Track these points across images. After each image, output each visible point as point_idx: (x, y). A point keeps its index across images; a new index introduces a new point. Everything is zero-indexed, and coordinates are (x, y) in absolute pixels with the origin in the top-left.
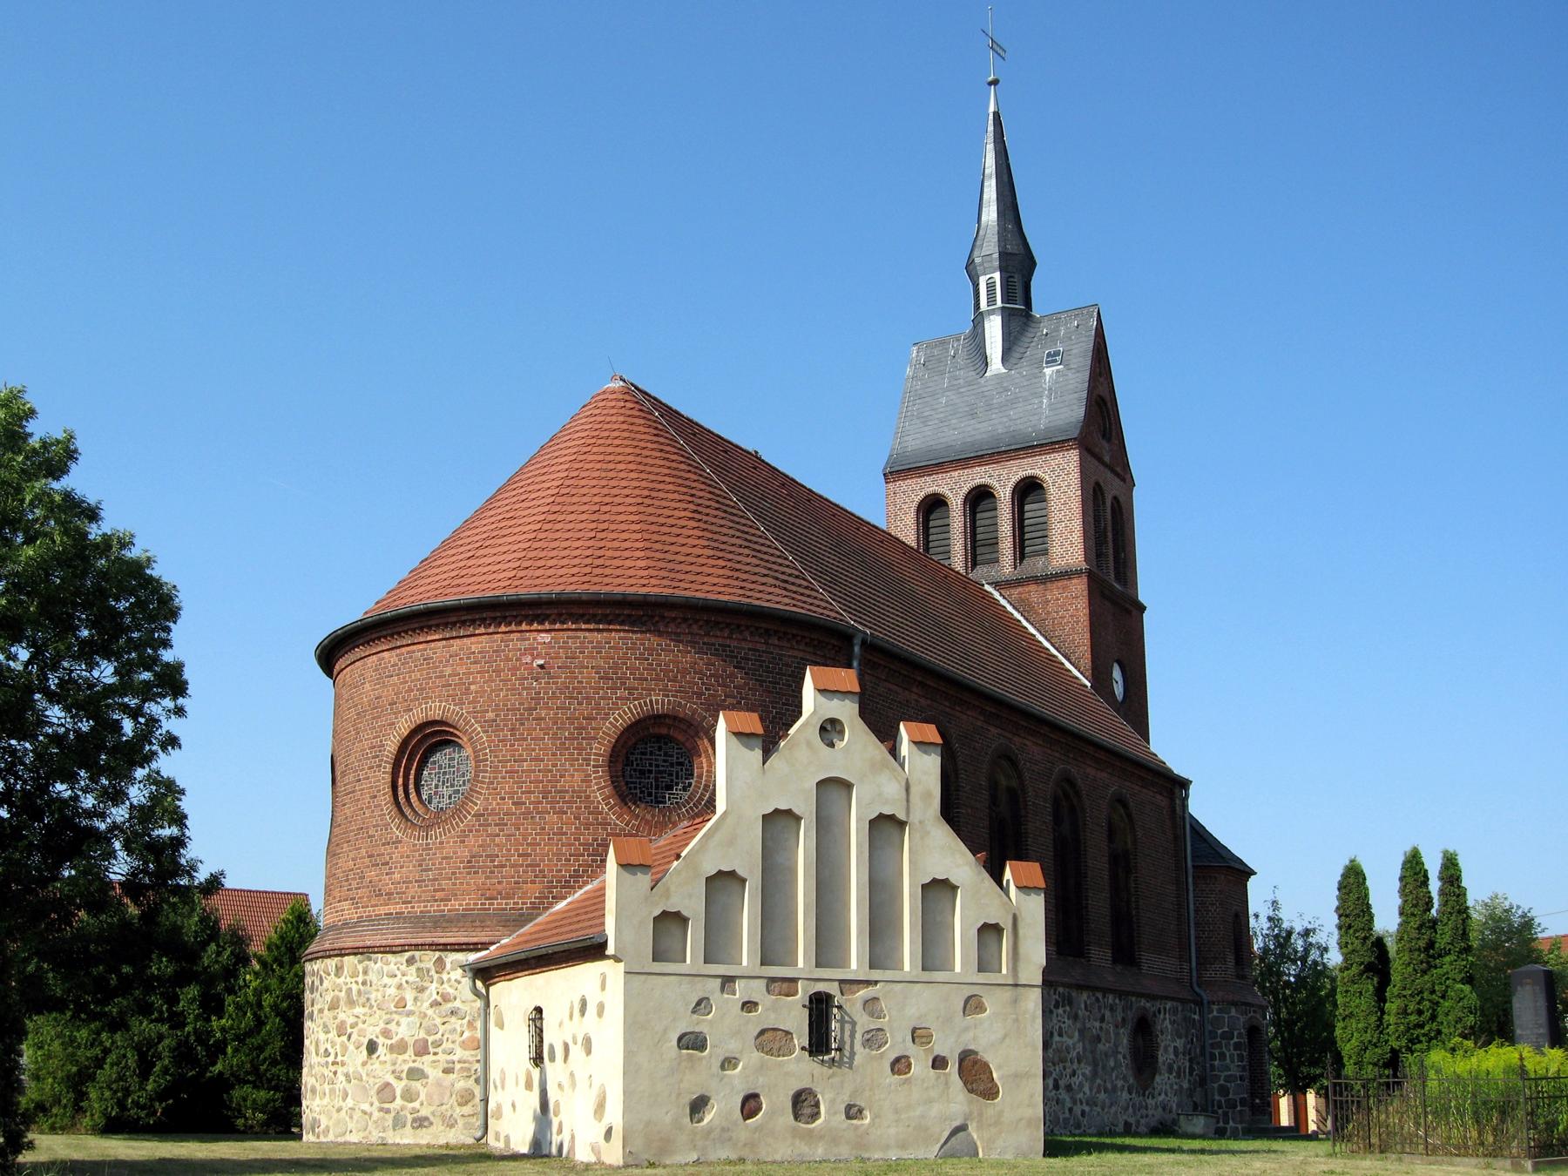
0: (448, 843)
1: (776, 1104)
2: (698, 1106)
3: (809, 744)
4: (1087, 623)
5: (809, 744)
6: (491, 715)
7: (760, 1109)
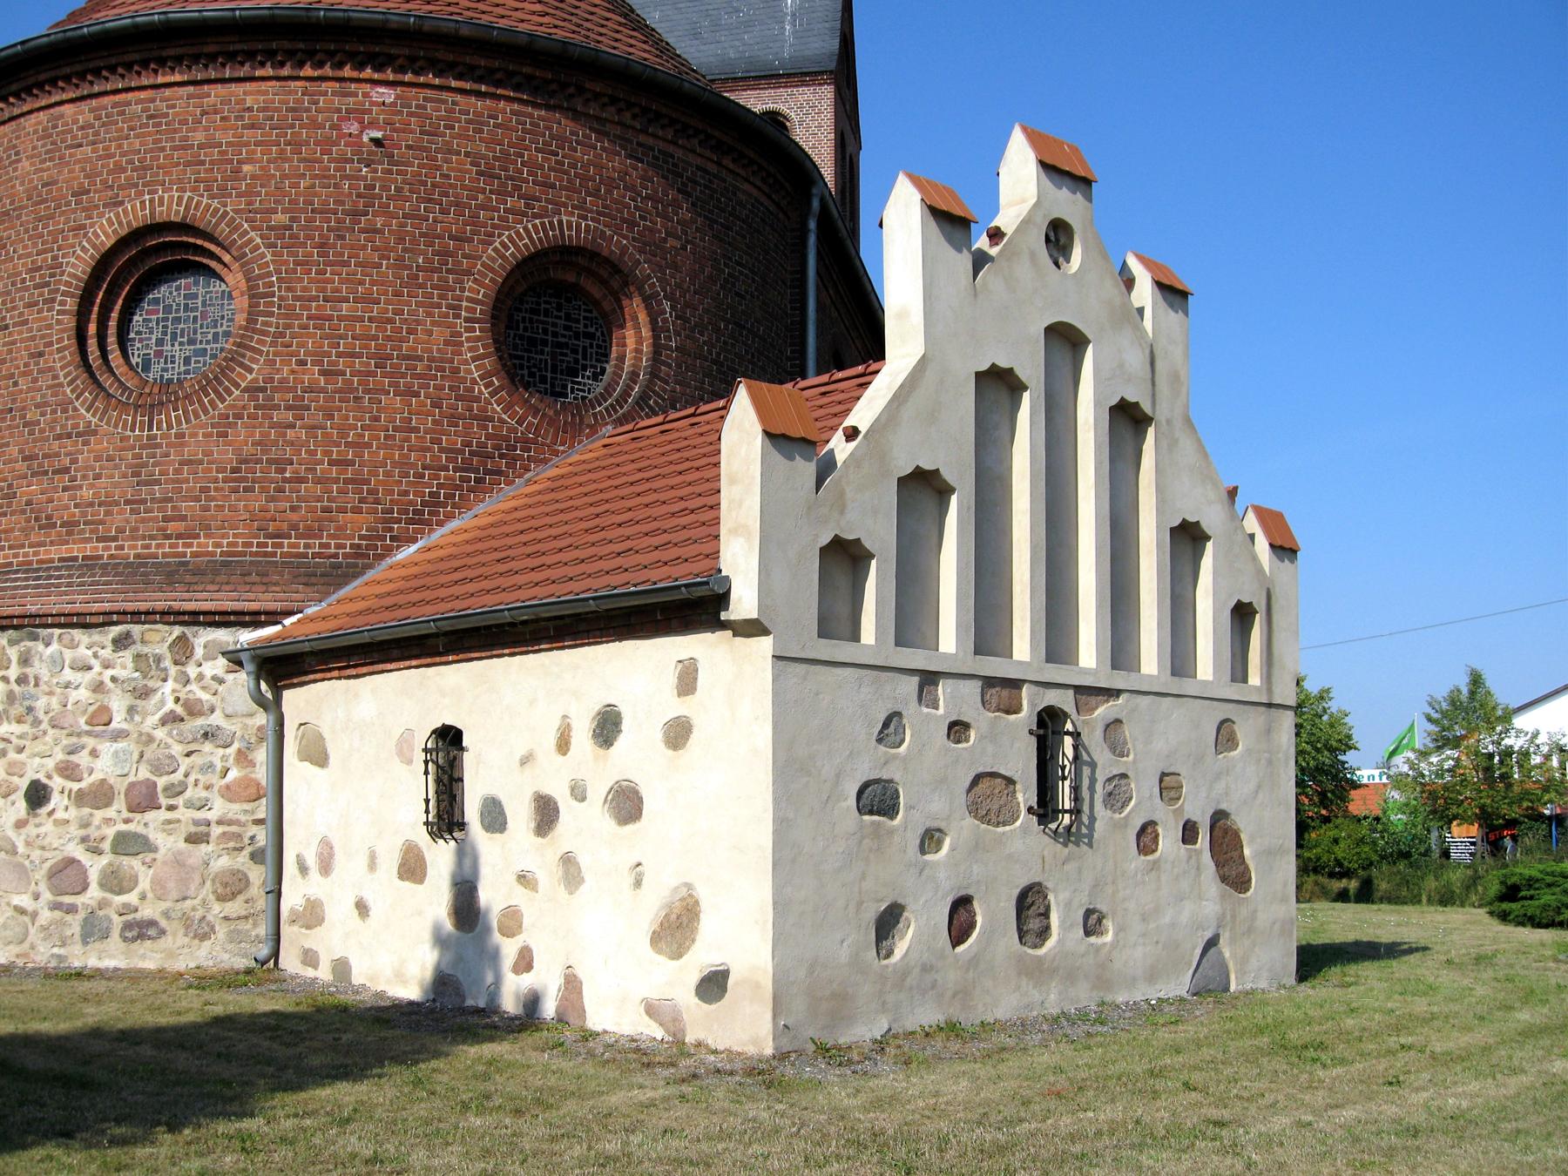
0: (191, 435)
2: (888, 922)
3: (1033, 256)
6: (280, 218)
7: (972, 925)
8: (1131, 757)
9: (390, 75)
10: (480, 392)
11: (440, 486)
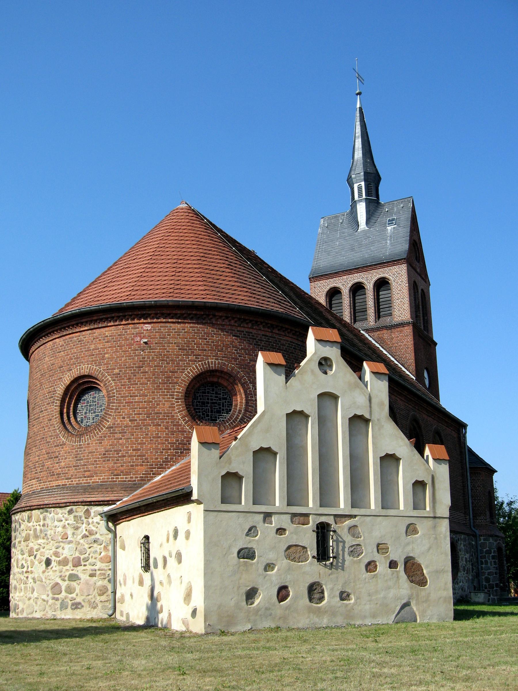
0: (93, 445)
1: (298, 592)
2: (251, 594)
3: (312, 371)
4: (413, 348)
5: (312, 371)
6: (116, 371)
7: (288, 595)
8: (362, 538)
9: (149, 321)
10: (181, 423)
11: (168, 455)
